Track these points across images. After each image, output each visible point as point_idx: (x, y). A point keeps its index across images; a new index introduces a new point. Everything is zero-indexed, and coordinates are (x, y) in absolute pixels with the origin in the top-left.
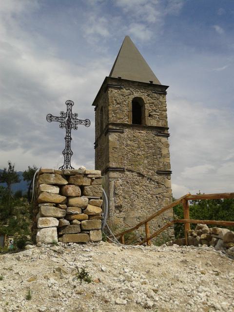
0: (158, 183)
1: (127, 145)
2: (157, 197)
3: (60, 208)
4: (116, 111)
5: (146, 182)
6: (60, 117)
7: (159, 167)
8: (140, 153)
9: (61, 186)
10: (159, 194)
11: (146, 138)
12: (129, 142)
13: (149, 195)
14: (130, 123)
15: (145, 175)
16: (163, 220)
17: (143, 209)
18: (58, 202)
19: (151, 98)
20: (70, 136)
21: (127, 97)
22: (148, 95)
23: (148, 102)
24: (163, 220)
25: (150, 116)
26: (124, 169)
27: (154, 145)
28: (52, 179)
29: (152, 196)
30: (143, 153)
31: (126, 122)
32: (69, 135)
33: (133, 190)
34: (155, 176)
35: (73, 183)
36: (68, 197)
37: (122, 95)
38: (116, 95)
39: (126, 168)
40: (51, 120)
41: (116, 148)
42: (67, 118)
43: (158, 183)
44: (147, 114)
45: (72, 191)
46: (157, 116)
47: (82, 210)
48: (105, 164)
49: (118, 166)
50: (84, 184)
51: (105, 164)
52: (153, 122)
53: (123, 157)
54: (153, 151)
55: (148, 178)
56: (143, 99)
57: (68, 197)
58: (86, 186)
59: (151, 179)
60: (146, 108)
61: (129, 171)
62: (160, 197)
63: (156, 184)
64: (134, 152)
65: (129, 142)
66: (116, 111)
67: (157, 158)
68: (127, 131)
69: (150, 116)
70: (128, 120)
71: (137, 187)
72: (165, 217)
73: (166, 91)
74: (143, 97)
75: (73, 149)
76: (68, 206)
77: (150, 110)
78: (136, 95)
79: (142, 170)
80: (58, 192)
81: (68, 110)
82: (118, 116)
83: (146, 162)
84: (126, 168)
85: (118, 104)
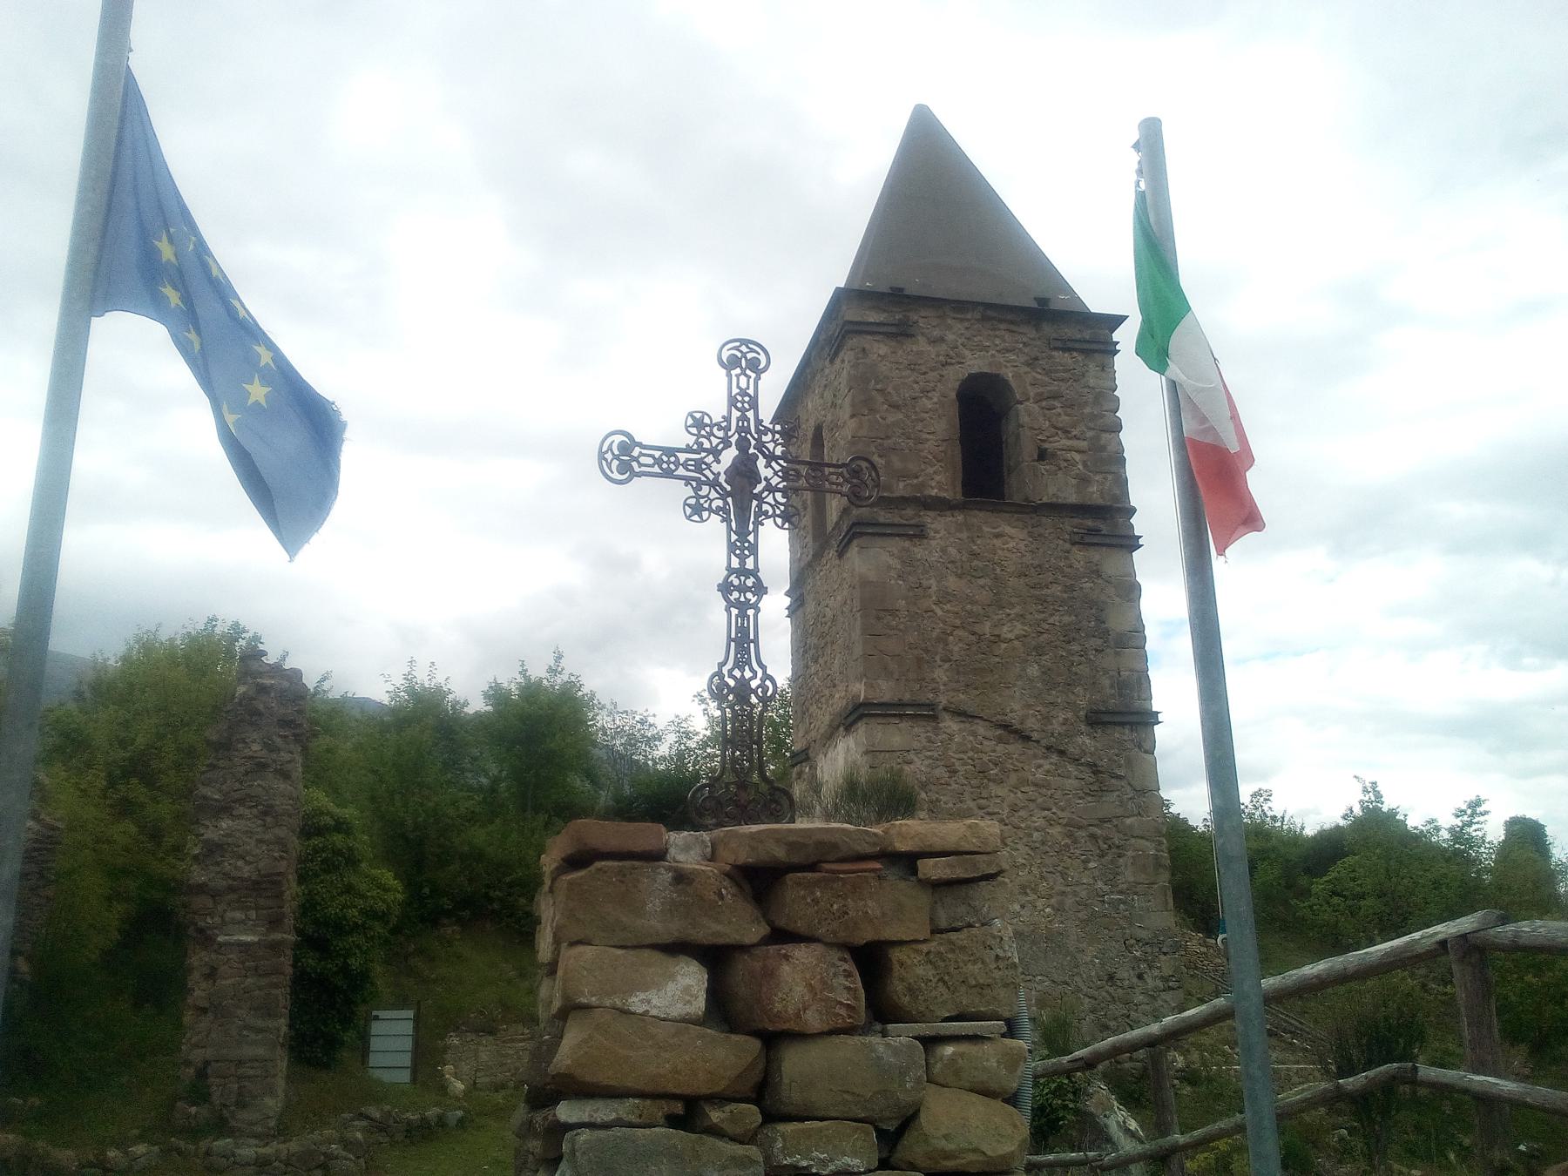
0: (1095, 769)
1: (945, 597)
2: (1093, 837)
3: (716, 1132)
4: (887, 443)
5: (1041, 767)
6: (688, 450)
7: (1097, 697)
8: (1005, 631)
9: (715, 958)
10: (1103, 821)
11: (1028, 559)
12: (952, 583)
13: (1059, 829)
14: (953, 493)
15: (1035, 736)
16: (1128, 948)
17: (1032, 897)
18: (701, 1086)
19: (1047, 373)
20: (754, 573)
21: (933, 375)
22: (1032, 362)
23: (1032, 392)
24: (1128, 948)
25: (1042, 455)
26: (931, 706)
27: (1069, 589)
28: (654, 905)
29: (1070, 835)
30: (1019, 628)
31: (934, 492)
32: (750, 563)
33: (980, 808)
34: (1079, 740)
35: (801, 926)
36: (773, 1040)
37: (912, 367)
38: (884, 368)
39: (943, 700)
40: (625, 468)
41: (893, 612)
42: (730, 455)
43: (1095, 769)
44: (1028, 450)
45: (799, 992)
46: (1077, 457)
47: (881, 1134)
48: (841, 687)
49: (907, 697)
50: (888, 934)
51: (841, 687)
52: (1060, 488)
53: (927, 651)
54: (1067, 619)
55: (1048, 748)
56: (1005, 383)
57: (773, 1040)
58: (901, 943)
59: (1062, 753)
60: (1025, 419)
61: (960, 714)
62: (1106, 839)
63: (1088, 776)
64: (977, 628)
65: (952, 583)
66: (887, 443)
67: (1084, 653)
68: (938, 524)
69: (1042, 455)
70: (941, 481)
71: (996, 790)
72: (1143, 934)
73: (1116, 336)
74: (1009, 374)
75: (718, 617)
76: (772, 1117)
77: (1041, 431)
78: (976, 363)
79: (1016, 708)
80: (699, 1005)
81: (668, 474)
82: (897, 463)
83: (1033, 671)
84: (943, 700)
85: (895, 407)
